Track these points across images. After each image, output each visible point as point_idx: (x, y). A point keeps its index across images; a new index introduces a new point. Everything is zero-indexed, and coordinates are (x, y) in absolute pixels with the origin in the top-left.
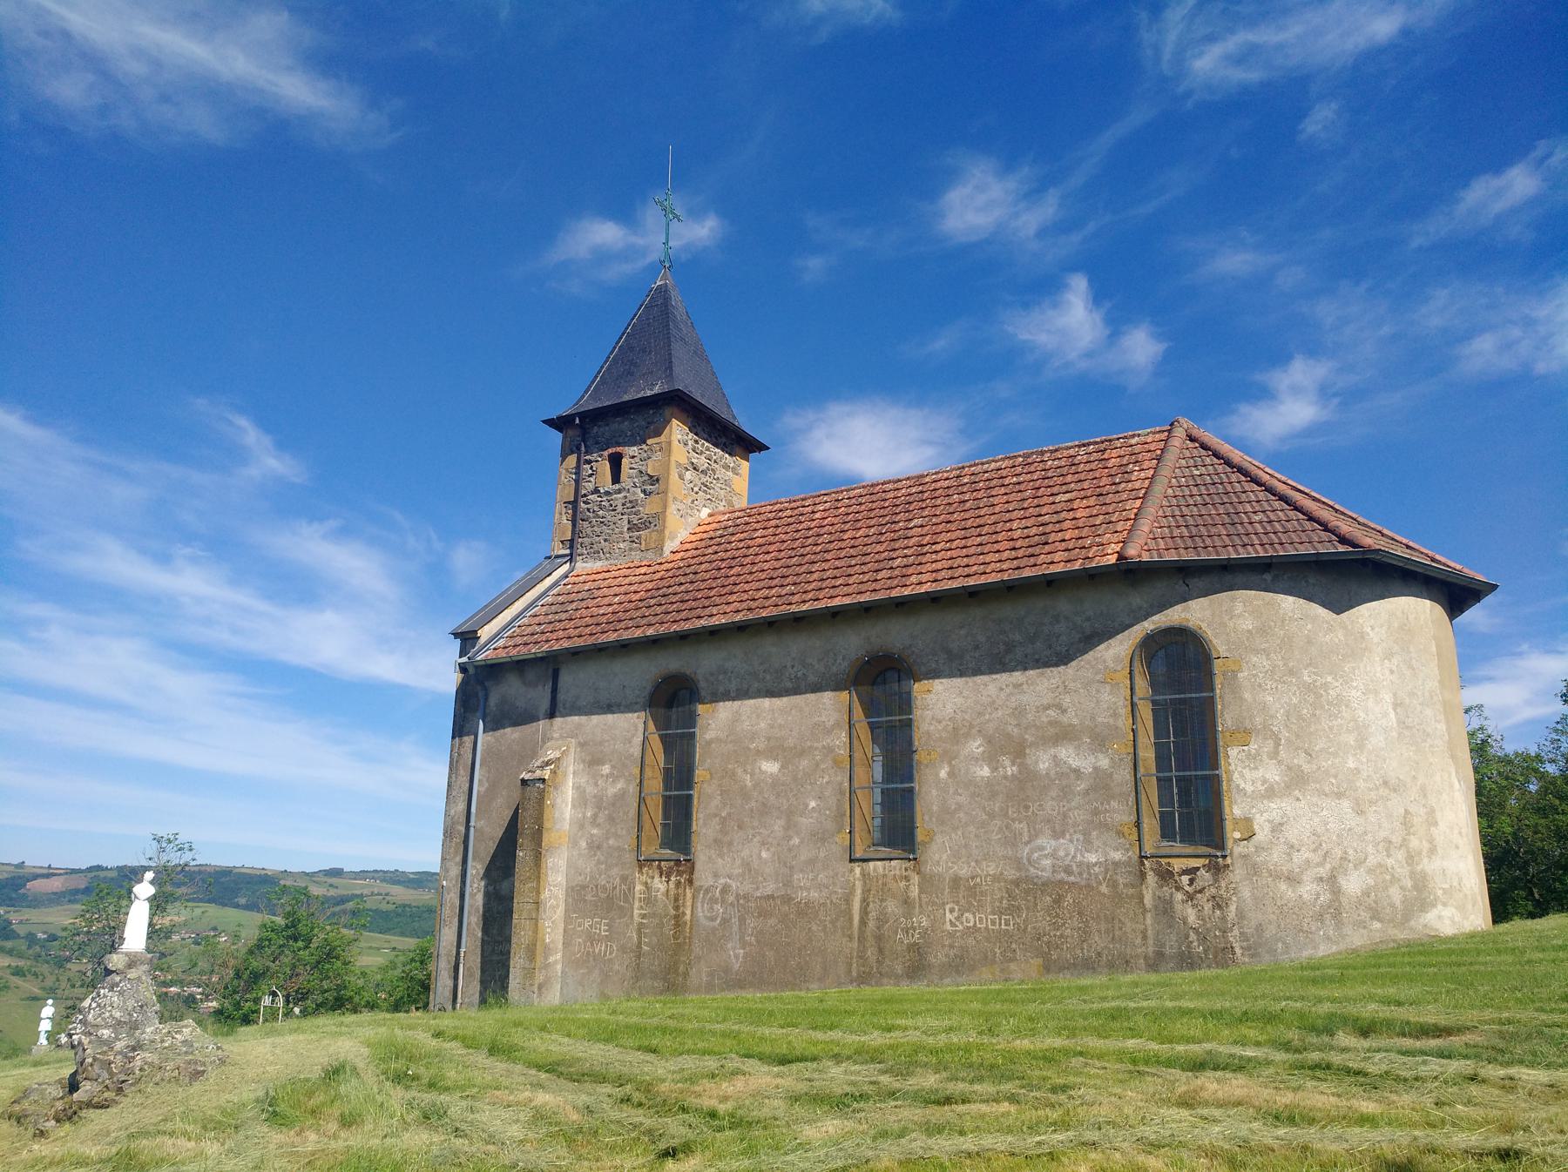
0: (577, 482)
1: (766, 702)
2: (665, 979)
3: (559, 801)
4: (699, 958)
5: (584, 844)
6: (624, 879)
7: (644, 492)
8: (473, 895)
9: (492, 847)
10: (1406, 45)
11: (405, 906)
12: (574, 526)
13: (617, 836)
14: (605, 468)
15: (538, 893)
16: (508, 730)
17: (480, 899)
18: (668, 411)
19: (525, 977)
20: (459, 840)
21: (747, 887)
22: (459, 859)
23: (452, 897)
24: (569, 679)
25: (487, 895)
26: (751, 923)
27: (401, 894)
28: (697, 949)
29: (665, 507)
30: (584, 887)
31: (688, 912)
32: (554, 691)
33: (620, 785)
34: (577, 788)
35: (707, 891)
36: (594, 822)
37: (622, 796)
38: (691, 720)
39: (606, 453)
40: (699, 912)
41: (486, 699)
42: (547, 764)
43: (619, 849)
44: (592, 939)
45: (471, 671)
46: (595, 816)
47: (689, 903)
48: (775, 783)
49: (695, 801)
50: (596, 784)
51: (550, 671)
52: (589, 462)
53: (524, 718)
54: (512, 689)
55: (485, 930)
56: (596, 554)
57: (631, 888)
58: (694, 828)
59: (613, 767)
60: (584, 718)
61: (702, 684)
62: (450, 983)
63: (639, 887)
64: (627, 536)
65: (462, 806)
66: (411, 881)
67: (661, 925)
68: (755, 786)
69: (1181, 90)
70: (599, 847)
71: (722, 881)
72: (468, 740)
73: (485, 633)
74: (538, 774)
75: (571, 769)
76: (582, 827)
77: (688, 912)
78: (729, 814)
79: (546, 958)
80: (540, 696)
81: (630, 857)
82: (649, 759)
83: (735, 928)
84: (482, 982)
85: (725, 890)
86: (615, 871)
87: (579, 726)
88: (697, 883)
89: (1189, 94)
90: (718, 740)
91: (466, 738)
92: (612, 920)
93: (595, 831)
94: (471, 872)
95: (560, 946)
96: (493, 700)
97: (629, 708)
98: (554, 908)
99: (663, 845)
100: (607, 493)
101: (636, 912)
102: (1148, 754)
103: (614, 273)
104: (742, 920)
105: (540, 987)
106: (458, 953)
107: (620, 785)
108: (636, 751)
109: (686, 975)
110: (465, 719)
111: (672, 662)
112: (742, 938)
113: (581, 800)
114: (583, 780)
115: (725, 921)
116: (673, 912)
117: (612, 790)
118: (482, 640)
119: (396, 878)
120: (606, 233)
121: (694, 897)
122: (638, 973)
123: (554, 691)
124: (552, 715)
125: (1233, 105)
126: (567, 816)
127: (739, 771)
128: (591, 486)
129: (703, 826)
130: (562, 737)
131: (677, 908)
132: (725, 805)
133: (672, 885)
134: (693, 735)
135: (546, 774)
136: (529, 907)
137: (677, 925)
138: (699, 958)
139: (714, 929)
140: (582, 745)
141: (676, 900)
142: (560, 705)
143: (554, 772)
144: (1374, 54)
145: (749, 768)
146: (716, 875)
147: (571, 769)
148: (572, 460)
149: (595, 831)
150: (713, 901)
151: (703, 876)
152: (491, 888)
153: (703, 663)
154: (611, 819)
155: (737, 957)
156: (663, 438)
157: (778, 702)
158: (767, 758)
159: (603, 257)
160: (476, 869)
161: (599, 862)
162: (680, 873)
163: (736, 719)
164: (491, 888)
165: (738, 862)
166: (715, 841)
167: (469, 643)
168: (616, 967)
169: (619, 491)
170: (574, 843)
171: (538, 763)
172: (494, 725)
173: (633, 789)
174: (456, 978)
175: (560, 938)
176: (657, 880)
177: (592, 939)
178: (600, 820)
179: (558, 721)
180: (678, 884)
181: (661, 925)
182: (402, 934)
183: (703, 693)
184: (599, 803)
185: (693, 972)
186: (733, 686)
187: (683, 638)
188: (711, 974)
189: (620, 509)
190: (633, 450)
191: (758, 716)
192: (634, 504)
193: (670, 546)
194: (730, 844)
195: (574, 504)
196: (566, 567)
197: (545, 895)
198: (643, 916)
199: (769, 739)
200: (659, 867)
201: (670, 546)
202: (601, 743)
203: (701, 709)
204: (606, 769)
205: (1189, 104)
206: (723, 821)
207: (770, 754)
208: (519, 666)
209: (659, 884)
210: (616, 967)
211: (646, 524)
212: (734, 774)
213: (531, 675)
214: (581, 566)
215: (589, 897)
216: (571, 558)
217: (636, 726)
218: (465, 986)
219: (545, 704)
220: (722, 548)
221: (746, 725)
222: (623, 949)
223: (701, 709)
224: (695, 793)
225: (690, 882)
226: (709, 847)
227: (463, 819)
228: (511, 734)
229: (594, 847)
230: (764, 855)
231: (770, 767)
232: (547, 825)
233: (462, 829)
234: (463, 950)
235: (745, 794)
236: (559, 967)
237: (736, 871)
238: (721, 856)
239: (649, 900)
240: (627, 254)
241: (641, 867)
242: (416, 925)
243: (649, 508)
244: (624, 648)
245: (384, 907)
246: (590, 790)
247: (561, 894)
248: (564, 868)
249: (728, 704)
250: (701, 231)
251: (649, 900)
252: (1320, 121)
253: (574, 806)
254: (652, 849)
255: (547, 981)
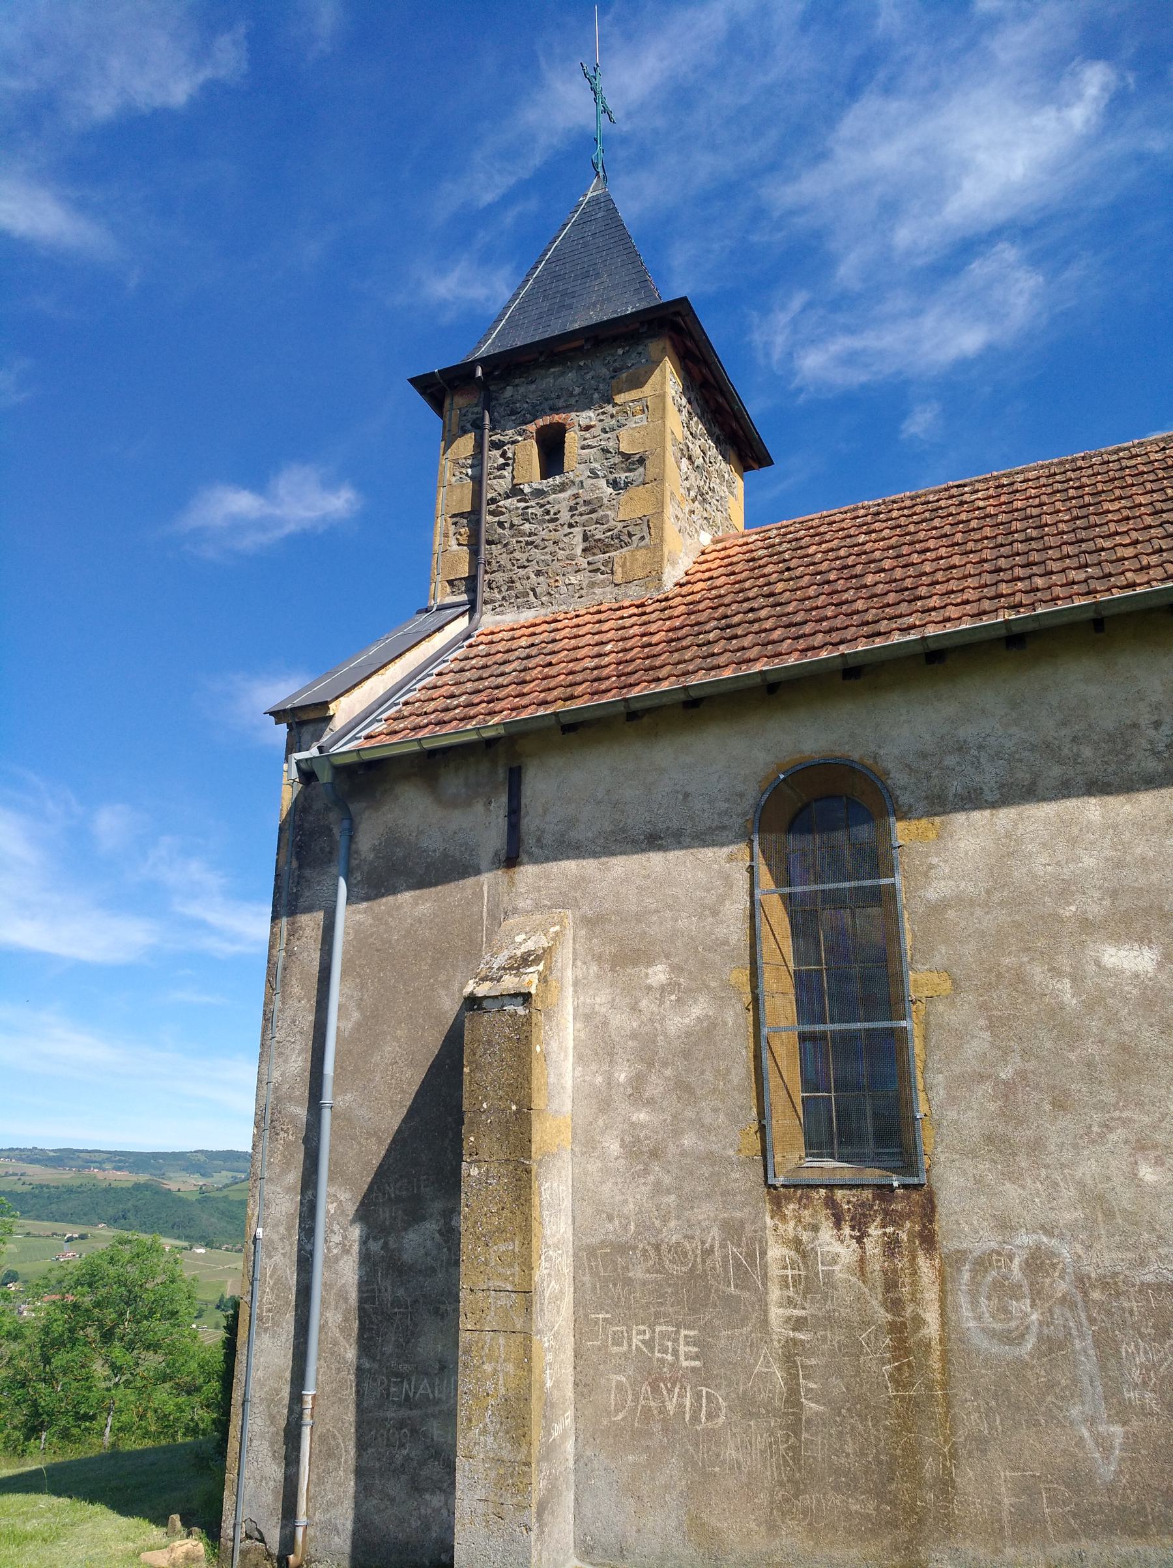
0: (477, 480)
1: (1092, 809)
2: (881, 1495)
3: (554, 1045)
4: (982, 1443)
5: (614, 1147)
6: (732, 1230)
7: (614, 484)
8: (331, 1262)
9: (376, 1152)
10: (990, 355)
11: (42, 1186)
12: (475, 552)
13: (702, 1128)
14: (529, 453)
15: (527, 1266)
16: (406, 897)
17: (349, 1272)
18: (654, 347)
19: (500, 1484)
20: (292, 1136)
21: (1105, 1258)
22: (294, 1177)
23: (280, 1264)
24: (548, 787)
25: (366, 1259)
26: (1137, 1355)
27: (39, 1174)
28: (971, 1418)
29: (661, 504)
30: (623, 1249)
31: (932, 1317)
32: (514, 812)
33: (699, 1009)
34: (586, 1016)
35: (982, 1264)
36: (637, 1092)
37: (708, 1030)
38: (877, 858)
39: (532, 428)
40: (959, 1316)
41: (351, 838)
42: (526, 960)
43: (710, 1158)
44: (655, 1378)
45: (325, 776)
46: (638, 1081)
47: (931, 1294)
48: (1150, 998)
49: (917, 1045)
50: (635, 1009)
51: (502, 774)
52: (497, 445)
53: (450, 868)
54: (411, 814)
55: (366, 1344)
56: (521, 598)
57: (756, 1253)
58: (922, 1109)
59: (676, 969)
60: (589, 866)
61: (899, 778)
62: (275, 1472)
63: (775, 1252)
64: (583, 562)
65: (297, 1063)
66: (50, 1159)
67: (853, 1349)
68: (1090, 1007)
69: (793, 386)
70: (655, 1154)
71: (1025, 1239)
72: (311, 922)
73: (343, 710)
74: (510, 983)
75: (569, 975)
76: (605, 1105)
77: (932, 1317)
78: (1022, 1074)
79: (548, 1431)
80: (485, 824)
81: (745, 1179)
82: (767, 948)
83: (1088, 1365)
84: (360, 1473)
85: (1038, 1262)
86: (704, 1212)
87: (581, 882)
88: (948, 1245)
89: (800, 390)
90: (960, 901)
91: (304, 919)
92: (708, 1329)
93: (642, 1116)
94: (325, 1207)
95: (569, 1393)
96: (368, 840)
97: (705, 837)
98: (557, 1298)
99: (815, 1147)
100: (539, 493)
101: (776, 1313)
102: (782, 1006)
103: (249, 542)
104: (1106, 1346)
105: (542, 1508)
106: (297, 1398)
107: (699, 1009)
108: (735, 931)
109: (946, 1485)
110: (300, 880)
111: (809, 736)
112: (1112, 1392)
113: (599, 1045)
114: (601, 1000)
115: (1053, 1347)
116: (884, 1316)
117: (677, 1023)
118: (338, 723)
119: (34, 1156)
120: (242, 503)
121: (943, 1279)
122: (797, 1474)
123: (514, 812)
124: (511, 859)
125: (848, 402)
126: (568, 1082)
127: (1037, 973)
128: (504, 485)
129: (949, 1103)
130: (538, 907)
131: (895, 1305)
132: (1006, 1052)
133: (872, 1246)
134: (885, 899)
135: (530, 980)
136: (503, 1300)
137: (901, 1348)
138: (982, 1443)
139: (1019, 1368)
140: (592, 923)
141: (891, 1285)
142: (529, 841)
143: (544, 980)
144: (963, 364)
145: (1064, 962)
146: (1004, 1225)
147: (569, 975)
148: (465, 445)
149: (642, 1116)
150: (1005, 1290)
151: (964, 1221)
152: (375, 1247)
153: (893, 733)
154: (683, 1088)
155: (1104, 1444)
156: (647, 390)
157: (1122, 807)
158: (1117, 939)
159: (238, 525)
160: (337, 1201)
161: (658, 1189)
162: (890, 1218)
163: (1010, 849)
164: (375, 1247)
165: (1069, 1193)
166: (989, 1139)
167: (307, 732)
168: (731, 1452)
169: (562, 488)
170: (587, 1143)
171: (501, 960)
172: (374, 884)
173: (735, 1017)
174: (291, 1459)
175: (568, 1374)
176: (827, 1233)
177: (655, 1378)
178: (655, 1087)
179: (528, 872)
180: (891, 1246)
181: (853, 1349)
182: (38, 1218)
183: (905, 799)
184: (647, 1050)
185: (967, 1477)
186: (989, 777)
187: (856, 675)
188: (1027, 1489)
189: (565, 516)
190: (587, 416)
191: (1073, 842)
192: (593, 506)
193: (672, 575)
194: (1036, 1146)
195: (473, 517)
196: (462, 623)
197: (541, 1271)
198: (799, 1324)
199: (1114, 894)
200: (830, 1203)
201: (672, 575)
202: (639, 917)
203: (902, 831)
204: (658, 974)
205: (802, 399)
206: (1006, 1091)
207: (1128, 924)
208: (429, 764)
209: (835, 1247)
210: (731, 1452)
211: (621, 539)
212: (1020, 979)
213: (453, 783)
214: (488, 620)
215: (638, 1273)
216: (472, 609)
217: (727, 879)
218: (318, 1481)
219: (494, 837)
220: (735, 594)
221: (1041, 864)
222: (747, 1406)
223: (902, 831)
224: (912, 1024)
225: (928, 1240)
226: (973, 1153)
227: (302, 1091)
228: (412, 906)
229: (643, 1153)
230: (1148, 1174)
231: (1131, 960)
232: (538, 1102)
233: (301, 1112)
234: (309, 1392)
235: (1069, 1032)
236: (570, 1446)
237: (1068, 1217)
238: (1015, 1177)
239: (808, 1281)
240: (262, 524)
241: (777, 1203)
242: (54, 1207)
243: (624, 510)
244: (695, 708)
245: (19, 1188)
246: (621, 1021)
247: (565, 1264)
248: (567, 1204)
249: (980, 817)
250: (340, 503)
251: (808, 1281)
252: (921, 422)
253: (580, 1058)
254: (790, 1158)
255: (553, 1488)
